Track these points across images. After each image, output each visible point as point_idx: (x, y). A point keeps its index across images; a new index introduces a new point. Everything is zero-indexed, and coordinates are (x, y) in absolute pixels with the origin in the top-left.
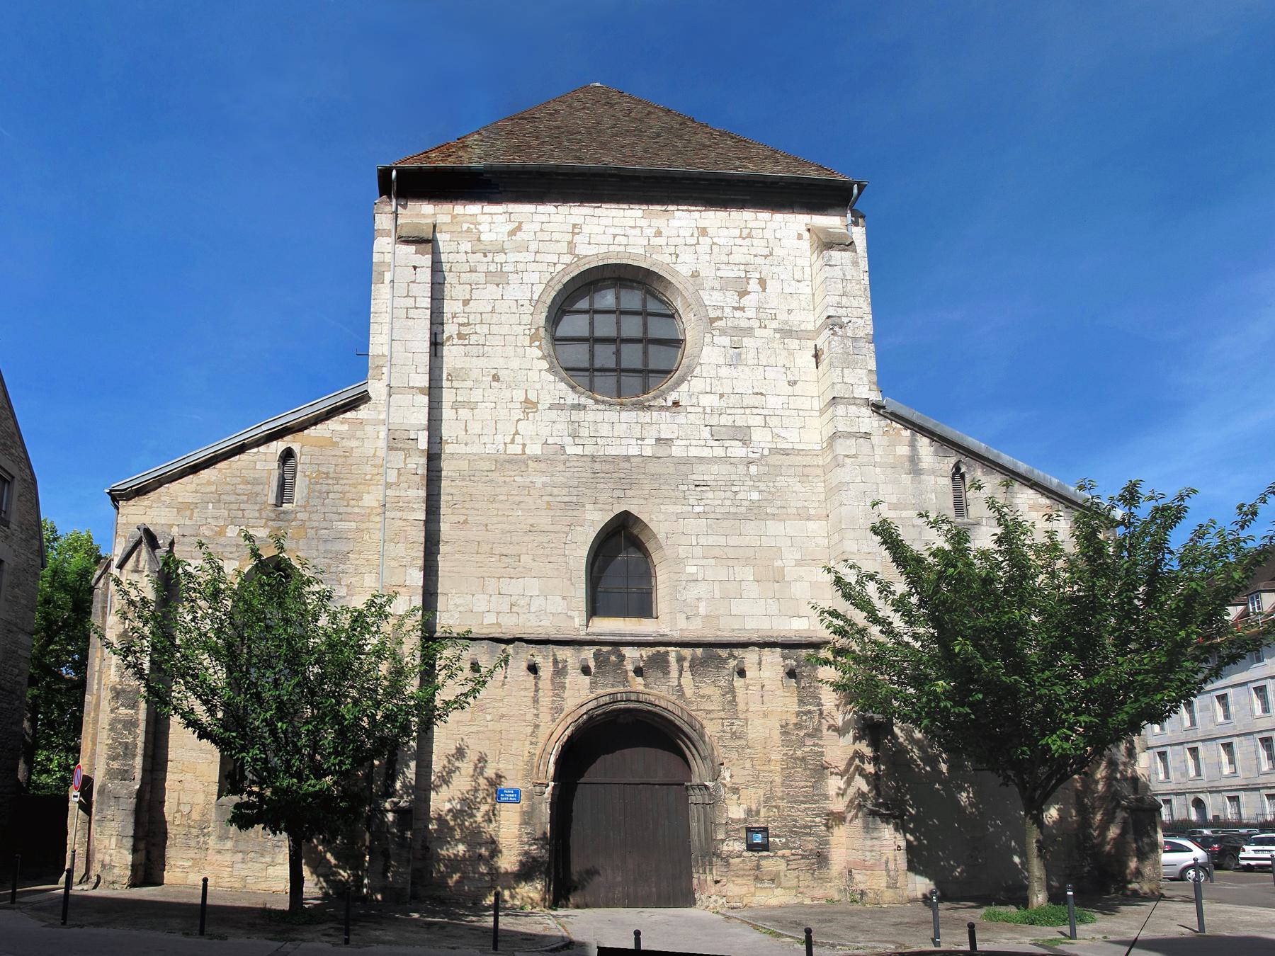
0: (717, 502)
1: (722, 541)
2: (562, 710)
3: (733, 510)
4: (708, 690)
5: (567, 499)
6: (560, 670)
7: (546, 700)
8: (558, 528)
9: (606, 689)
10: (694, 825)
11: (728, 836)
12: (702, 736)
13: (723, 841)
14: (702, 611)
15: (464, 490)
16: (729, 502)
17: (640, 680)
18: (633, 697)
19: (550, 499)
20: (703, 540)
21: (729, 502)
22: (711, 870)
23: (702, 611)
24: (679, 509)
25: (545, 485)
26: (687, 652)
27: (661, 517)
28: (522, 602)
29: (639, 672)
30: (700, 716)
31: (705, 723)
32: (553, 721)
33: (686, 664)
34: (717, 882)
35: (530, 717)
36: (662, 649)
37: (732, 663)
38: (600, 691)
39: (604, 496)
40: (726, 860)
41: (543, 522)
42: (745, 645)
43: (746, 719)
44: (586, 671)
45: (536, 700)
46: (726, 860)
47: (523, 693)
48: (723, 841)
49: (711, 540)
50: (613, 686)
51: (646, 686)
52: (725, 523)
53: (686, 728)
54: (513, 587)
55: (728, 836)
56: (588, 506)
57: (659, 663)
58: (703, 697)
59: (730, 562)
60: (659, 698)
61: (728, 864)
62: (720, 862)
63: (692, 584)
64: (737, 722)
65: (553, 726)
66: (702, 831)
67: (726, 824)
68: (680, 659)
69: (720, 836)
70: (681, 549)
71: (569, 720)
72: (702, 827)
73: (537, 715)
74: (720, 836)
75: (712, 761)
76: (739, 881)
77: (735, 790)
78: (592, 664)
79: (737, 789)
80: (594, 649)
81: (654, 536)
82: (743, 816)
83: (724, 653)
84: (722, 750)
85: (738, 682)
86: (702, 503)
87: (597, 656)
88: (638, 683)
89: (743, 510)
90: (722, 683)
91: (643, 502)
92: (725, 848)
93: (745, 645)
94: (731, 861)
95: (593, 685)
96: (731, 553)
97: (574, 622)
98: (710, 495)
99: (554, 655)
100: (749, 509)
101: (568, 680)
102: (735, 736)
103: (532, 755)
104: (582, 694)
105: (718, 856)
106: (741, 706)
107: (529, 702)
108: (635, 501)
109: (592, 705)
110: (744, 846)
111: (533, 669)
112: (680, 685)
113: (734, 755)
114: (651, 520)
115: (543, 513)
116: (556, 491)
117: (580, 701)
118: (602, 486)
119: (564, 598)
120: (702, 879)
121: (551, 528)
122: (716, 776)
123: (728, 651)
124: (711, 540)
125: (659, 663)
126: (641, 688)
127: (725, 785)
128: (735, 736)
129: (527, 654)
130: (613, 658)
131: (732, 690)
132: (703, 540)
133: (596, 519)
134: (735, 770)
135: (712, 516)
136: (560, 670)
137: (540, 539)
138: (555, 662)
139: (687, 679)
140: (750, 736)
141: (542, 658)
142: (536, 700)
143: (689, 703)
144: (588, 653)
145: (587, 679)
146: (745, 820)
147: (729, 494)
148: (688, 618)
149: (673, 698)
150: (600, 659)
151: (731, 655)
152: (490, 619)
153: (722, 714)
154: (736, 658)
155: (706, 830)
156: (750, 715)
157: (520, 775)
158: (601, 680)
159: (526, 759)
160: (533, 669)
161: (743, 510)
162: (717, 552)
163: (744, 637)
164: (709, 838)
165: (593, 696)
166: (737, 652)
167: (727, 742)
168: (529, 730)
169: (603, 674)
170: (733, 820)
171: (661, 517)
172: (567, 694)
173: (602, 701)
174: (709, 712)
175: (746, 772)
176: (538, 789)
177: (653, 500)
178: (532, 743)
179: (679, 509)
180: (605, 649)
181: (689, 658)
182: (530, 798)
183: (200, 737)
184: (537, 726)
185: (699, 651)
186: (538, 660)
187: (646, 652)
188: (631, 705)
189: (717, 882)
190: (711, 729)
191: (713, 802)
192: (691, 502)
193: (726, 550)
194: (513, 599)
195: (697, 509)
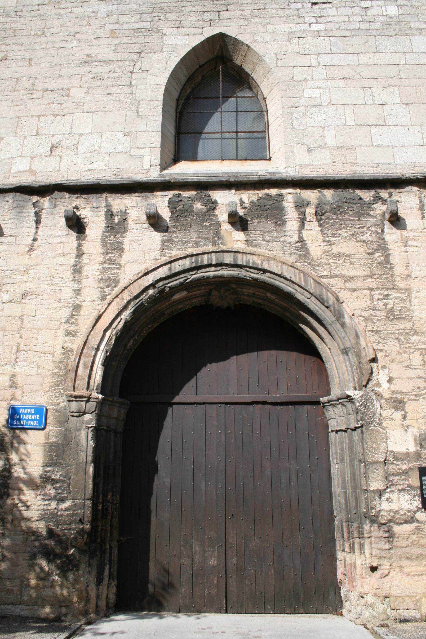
0: (342, 19)
1: (353, 59)
2: (116, 282)
3: (364, 26)
4: (344, 246)
5: (137, 26)
6: (116, 226)
7: (93, 266)
8: (124, 56)
9: (187, 247)
10: (335, 467)
11: (389, 484)
12: (339, 316)
13: (380, 493)
14: (331, 141)
15: (8, 26)
16: (359, 19)
17: (240, 235)
18: (228, 259)
19: (116, 27)
20: (325, 59)
21: (359, 19)
22: (362, 547)
23: (331, 141)
24: (292, 28)
25: (109, 14)
26: (312, 195)
27: (268, 37)
28: (66, 143)
29: (239, 222)
30: (336, 284)
31: (342, 296)
32: (103, 298)
33: (310, 211)
34: (373, 569)
35: (67, 294)
36: (274, 191)
37: (380, 209)
38: (176, 253)
39: (189, 21)
40: (387, 527)
41: (104, 51)
42: (398, 183)
43: (408, 290)
44: (155, 221)
45: (77, 270)
46: (387, 527)
47: (59, 260)
48: (380, 493)
49: (336, 59)
50: (197, 244)
51: (248, 242)
52: (354, 40)
53: (313, 305)
54: (57, 128)
55: (389, 484)
56: (77, 93)
57: (272, 212)
58: (338, 256)
59: (366, 83)
60: (269, 259)
61: (391, 536)
62: (376, 532)
63: (314, 110)
64: (394, 294)
65: (102, 307)
66: (348, 478)
67: (385, 462)
68: (300, 206)
69: (376, 484)
70: (296, 71)
71: (127, 296)
72: (348, 470)
73: (77, 291)
74: (376, 484)
75: (358, 355)
76: (412, 567)
77: (398, 404)
78: (165, 214)
79: (401, 402)
80: (170, 194)
81: (260, 58)
82: (412, 448)
83: (367, 195)
84: (373, 337)
85: (392, 234)
86: (323, 20)
87: (172, 205)
88: (235, 239)
89: (378, 25)
90: (367, 237)
91: (243, 22)
92: (385, 506)
93: (398, 183)
94: (396, 529)
95: (165, 245)
96: (366, 72)
97: (147, 165)
98: (333, 12)
99: (108, 206)
100: (387, 24)
101: (128, 240)
102: (392, 315)
103: (66, 351)
104: (145, 256)
105: (374, 520)
106: (399, 270)
107: (67, 272)
108: (233, 23)
109: (163, 272)
110: (418, 502)
111: (76, 224)
112: (301, 240)
113: (392, 346)
114: (255, 41)
115: (106, 41)
116: (124, 19)
117: (142, 268)
118: (188, 9)
119: (126, 134)
120: (351, 561)
121: (115, 57)
122: (366, 381)
123: (372, 193)
124: (336, 59)
125: (272, 212)
126: (240, 246)
127: (379, 395)
128: (392, 315)
129: (68, 203)
130: (198, 206)
131: (383, 247)
132: (325, 59)
133: (180, 42)
134: (396, 370)
135: (336, 33)
136: (116, 226)
137: (99, 69)
138: (110, 215)
139: (312, 232)
140: (417, 315)
141: (92, 212)
142: (77, 270)
143: (316, 266)
144: (161, 202)
145: (157, 237)
146: (418, 456)
147: (357, 10)
148: (310, 150)
149: (291, 259)
150: (179, 211)
151: (378, 198)
152: (21, 165)
153: (370, 282)
154: (384, 201)
155: (353, 475)
156: (414, 284)
157: (48, 383)
158: (178, 236)
159: (58, 357)
160: (76, 224)
161: (378, 25)
162: (346, 72)
163: (395, 172)
164: (357, 488)
165: (164, 259)
166: (384, 194)
167: (380, 325)
168: (66, 313)
169: (182, 229)
170: (397, 457)
171: (268, 37)
172: (126, 258)
173: (177, 267)
174: (348, 279)
175: (413, 373)
176: (74, 406)
177: (257, 20)
178: (68, 334)
179: (292, 28)
180: (186, 194)
181: (314, 202)
182: (62, 420)
183: (397, 391)
184: (77, 308)
185: (329, 194)
186: (83, 213)
187: (248, 197)
188: (226, 272)
189: (373, 569)
190: (353, 305)
191: (363, 425)
192: (307, 20)
193: (359, 69)
194: (55, 140)
195: (315, 27)
